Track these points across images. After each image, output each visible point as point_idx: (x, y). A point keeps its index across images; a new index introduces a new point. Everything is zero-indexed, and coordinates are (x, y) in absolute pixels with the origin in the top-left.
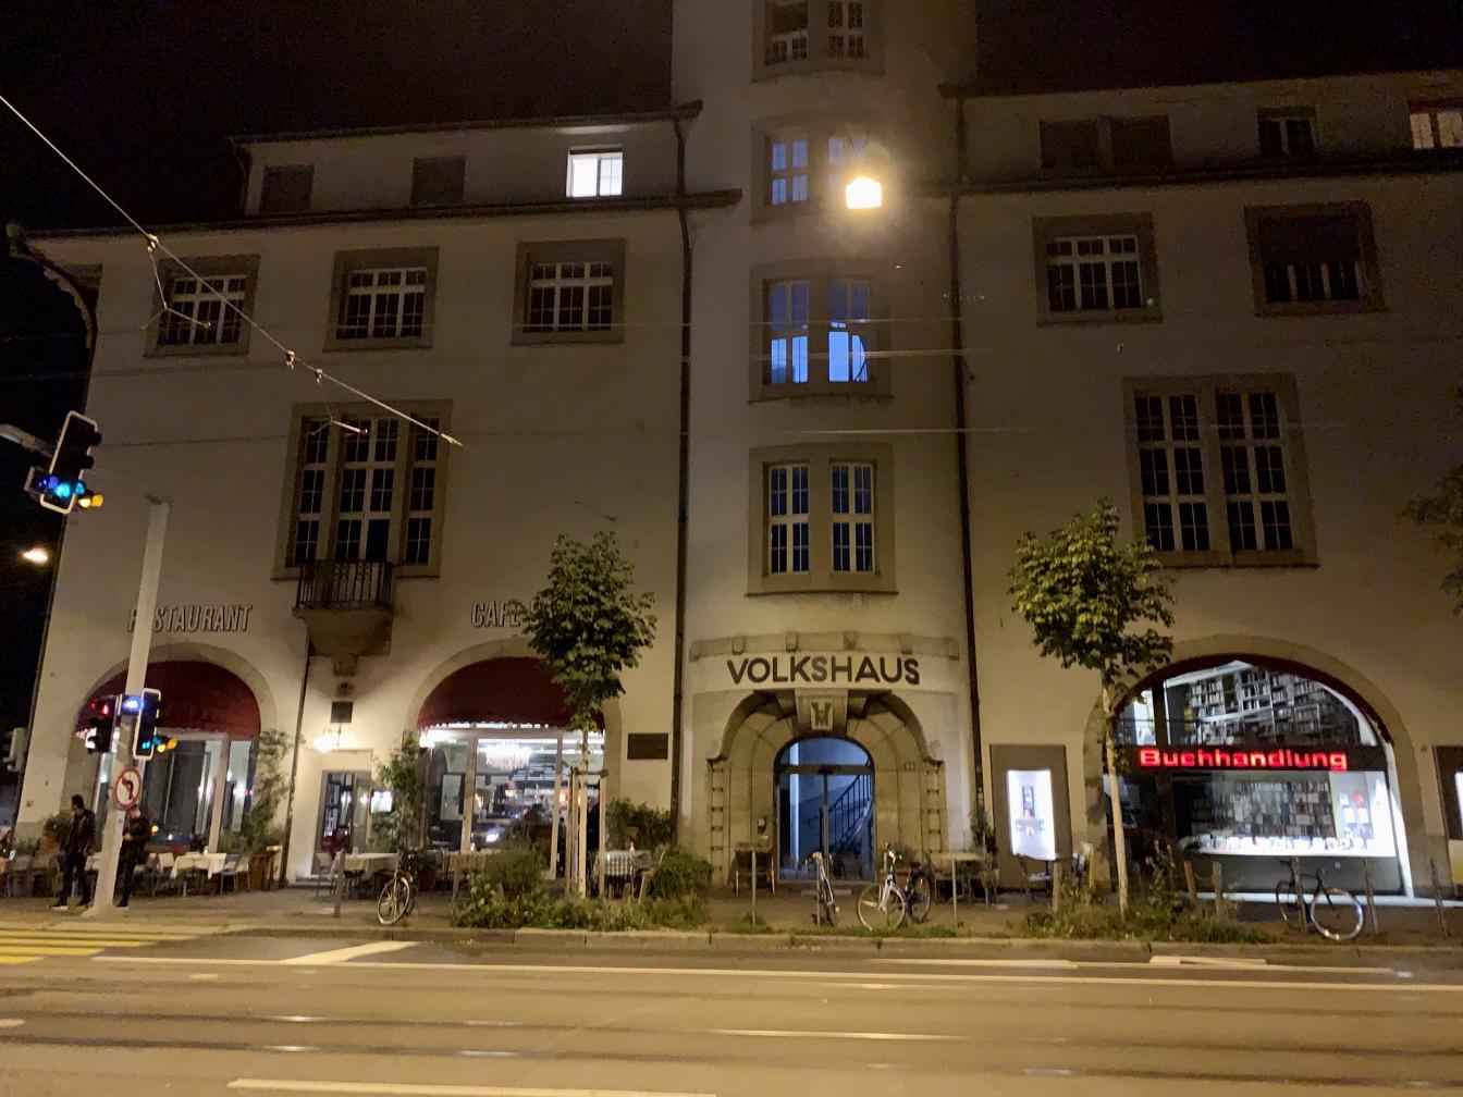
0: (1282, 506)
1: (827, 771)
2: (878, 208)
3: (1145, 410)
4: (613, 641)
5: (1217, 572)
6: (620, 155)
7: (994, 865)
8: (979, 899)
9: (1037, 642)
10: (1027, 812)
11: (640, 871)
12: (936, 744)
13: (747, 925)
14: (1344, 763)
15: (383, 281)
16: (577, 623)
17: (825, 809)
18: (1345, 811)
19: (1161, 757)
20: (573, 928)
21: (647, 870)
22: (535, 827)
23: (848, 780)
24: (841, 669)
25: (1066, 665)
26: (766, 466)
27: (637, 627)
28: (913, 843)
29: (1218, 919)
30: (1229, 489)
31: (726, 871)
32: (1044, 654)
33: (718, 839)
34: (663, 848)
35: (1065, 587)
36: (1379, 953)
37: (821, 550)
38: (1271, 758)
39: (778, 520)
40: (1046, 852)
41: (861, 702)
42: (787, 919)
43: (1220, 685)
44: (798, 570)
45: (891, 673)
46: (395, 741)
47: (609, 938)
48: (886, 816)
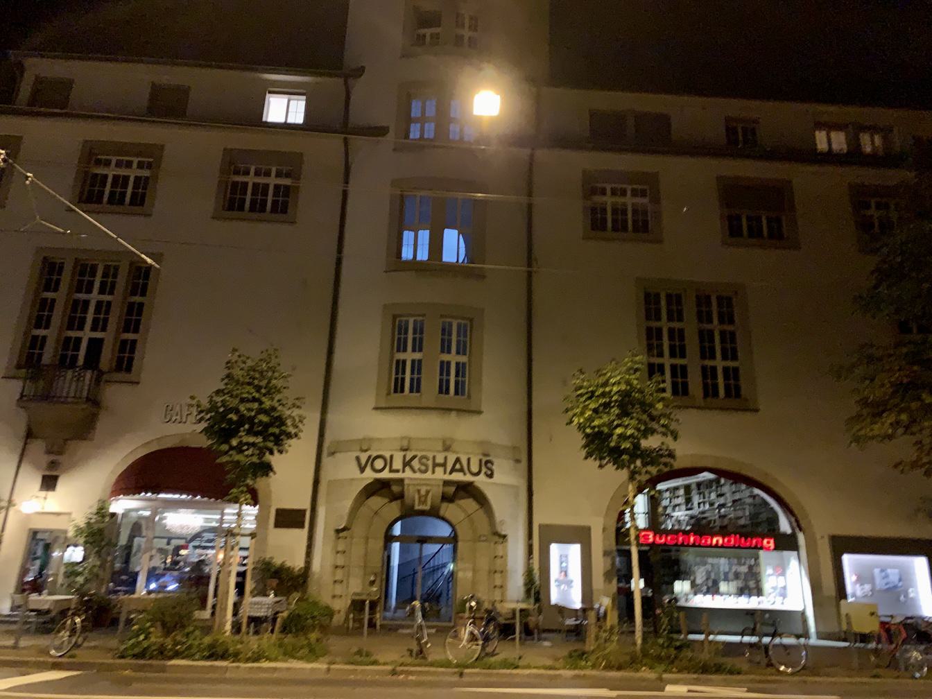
0: (736, 370)
1: (423, 540)
2: (502, 99)
3: (650, 304)
4: (270, 432)
5: (694, 411)
6: (304, 97)
7: (540, 611)
8: (529, 637)
9: (585, 446)
10: (563, 573)
11: (277, 613)
12: (502, 522)
13: (357, 658)
14: (772, 545)
15: (119, 164)
16: (242, 417)
17: (419, 569)
18: (770, 581)
19: (654, 537)
20: (216, 660)
21: (282, 612)
22: (197, 579)
23: (438, 546)
24: (439, 465)
25: (601, 466)
26: (395, 317)
27: (289, 422)
28: (483, 594)
29: (705, 656)
30: (703, 357)
31: (343, 614)
32: (586, 458)
33: (338, 590)
34: (296, 596)
35: (605, 408)
36: (820, 683)
37: (430, 382)
38: (726, 540)
39: (401, 356)
40: (574, 603)
41: (452, 489)
42: (390, 653)
43: (682, 492)
44: (413, 392)
45: (475, 469)
46: (91, 507)
47: (246, 668)
48: (465, 576)
